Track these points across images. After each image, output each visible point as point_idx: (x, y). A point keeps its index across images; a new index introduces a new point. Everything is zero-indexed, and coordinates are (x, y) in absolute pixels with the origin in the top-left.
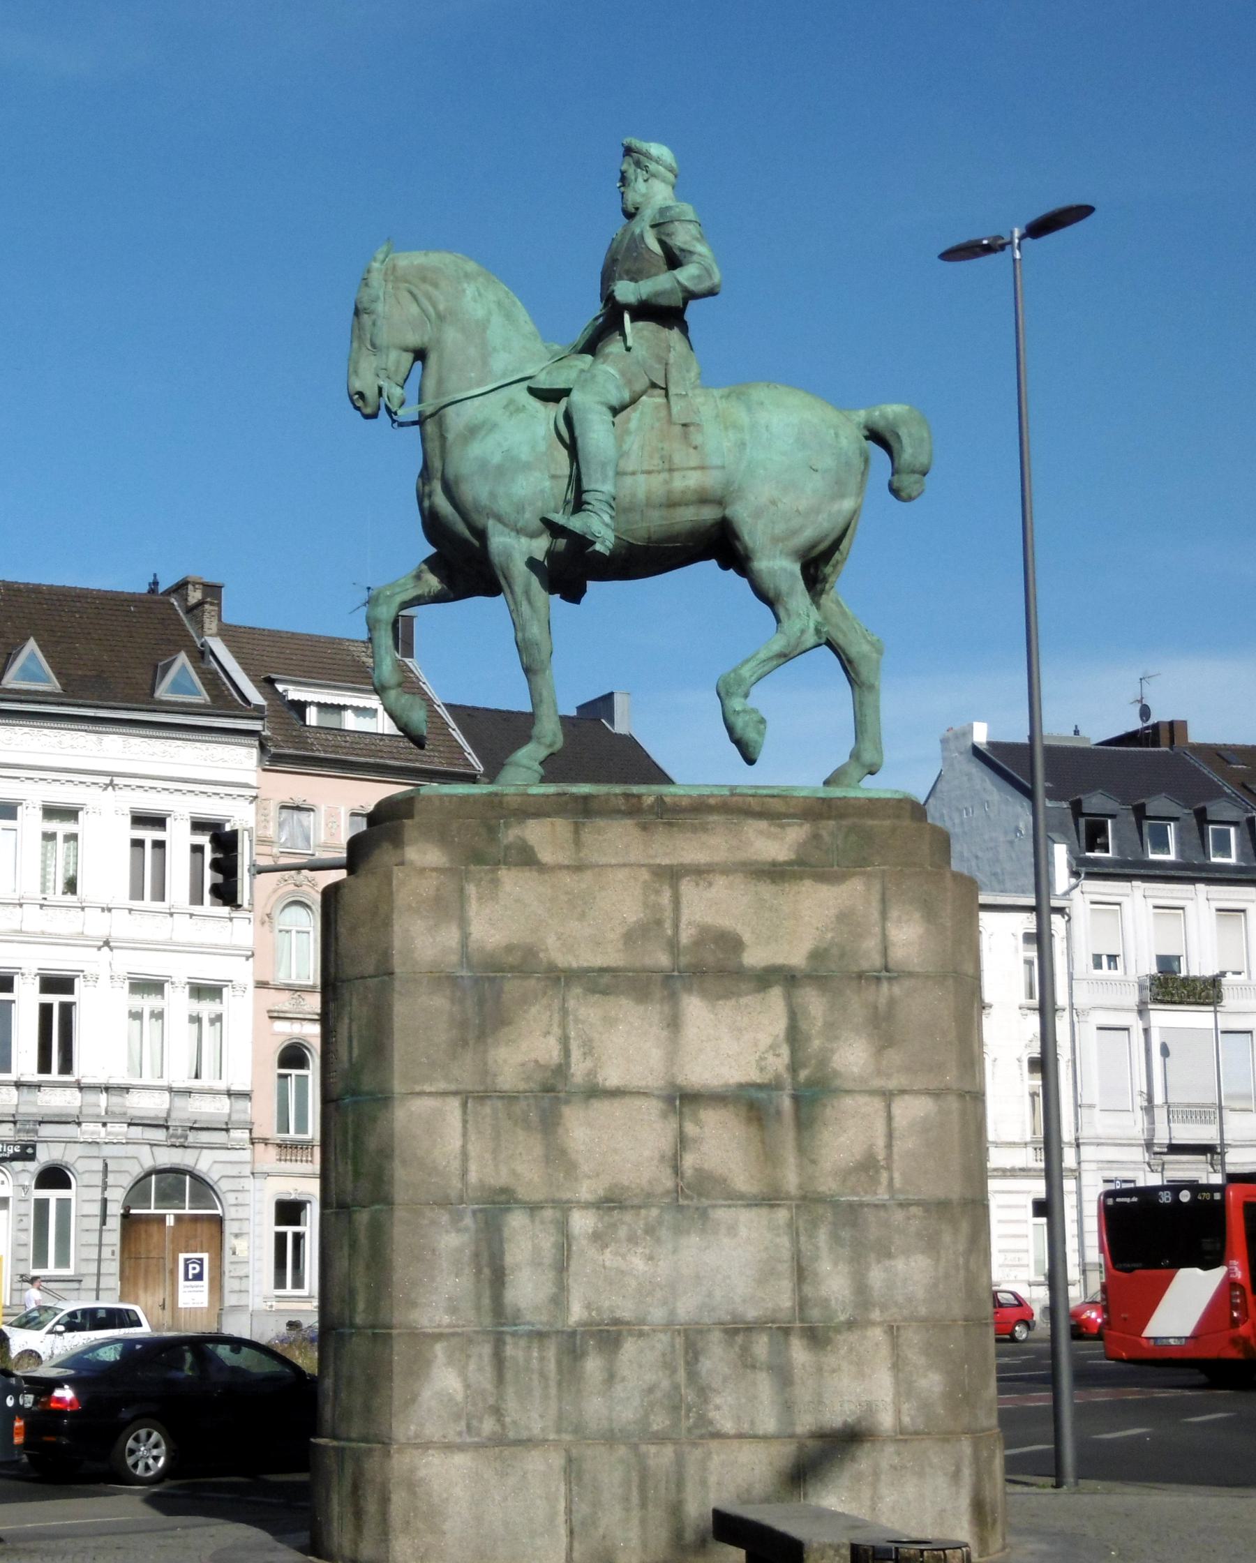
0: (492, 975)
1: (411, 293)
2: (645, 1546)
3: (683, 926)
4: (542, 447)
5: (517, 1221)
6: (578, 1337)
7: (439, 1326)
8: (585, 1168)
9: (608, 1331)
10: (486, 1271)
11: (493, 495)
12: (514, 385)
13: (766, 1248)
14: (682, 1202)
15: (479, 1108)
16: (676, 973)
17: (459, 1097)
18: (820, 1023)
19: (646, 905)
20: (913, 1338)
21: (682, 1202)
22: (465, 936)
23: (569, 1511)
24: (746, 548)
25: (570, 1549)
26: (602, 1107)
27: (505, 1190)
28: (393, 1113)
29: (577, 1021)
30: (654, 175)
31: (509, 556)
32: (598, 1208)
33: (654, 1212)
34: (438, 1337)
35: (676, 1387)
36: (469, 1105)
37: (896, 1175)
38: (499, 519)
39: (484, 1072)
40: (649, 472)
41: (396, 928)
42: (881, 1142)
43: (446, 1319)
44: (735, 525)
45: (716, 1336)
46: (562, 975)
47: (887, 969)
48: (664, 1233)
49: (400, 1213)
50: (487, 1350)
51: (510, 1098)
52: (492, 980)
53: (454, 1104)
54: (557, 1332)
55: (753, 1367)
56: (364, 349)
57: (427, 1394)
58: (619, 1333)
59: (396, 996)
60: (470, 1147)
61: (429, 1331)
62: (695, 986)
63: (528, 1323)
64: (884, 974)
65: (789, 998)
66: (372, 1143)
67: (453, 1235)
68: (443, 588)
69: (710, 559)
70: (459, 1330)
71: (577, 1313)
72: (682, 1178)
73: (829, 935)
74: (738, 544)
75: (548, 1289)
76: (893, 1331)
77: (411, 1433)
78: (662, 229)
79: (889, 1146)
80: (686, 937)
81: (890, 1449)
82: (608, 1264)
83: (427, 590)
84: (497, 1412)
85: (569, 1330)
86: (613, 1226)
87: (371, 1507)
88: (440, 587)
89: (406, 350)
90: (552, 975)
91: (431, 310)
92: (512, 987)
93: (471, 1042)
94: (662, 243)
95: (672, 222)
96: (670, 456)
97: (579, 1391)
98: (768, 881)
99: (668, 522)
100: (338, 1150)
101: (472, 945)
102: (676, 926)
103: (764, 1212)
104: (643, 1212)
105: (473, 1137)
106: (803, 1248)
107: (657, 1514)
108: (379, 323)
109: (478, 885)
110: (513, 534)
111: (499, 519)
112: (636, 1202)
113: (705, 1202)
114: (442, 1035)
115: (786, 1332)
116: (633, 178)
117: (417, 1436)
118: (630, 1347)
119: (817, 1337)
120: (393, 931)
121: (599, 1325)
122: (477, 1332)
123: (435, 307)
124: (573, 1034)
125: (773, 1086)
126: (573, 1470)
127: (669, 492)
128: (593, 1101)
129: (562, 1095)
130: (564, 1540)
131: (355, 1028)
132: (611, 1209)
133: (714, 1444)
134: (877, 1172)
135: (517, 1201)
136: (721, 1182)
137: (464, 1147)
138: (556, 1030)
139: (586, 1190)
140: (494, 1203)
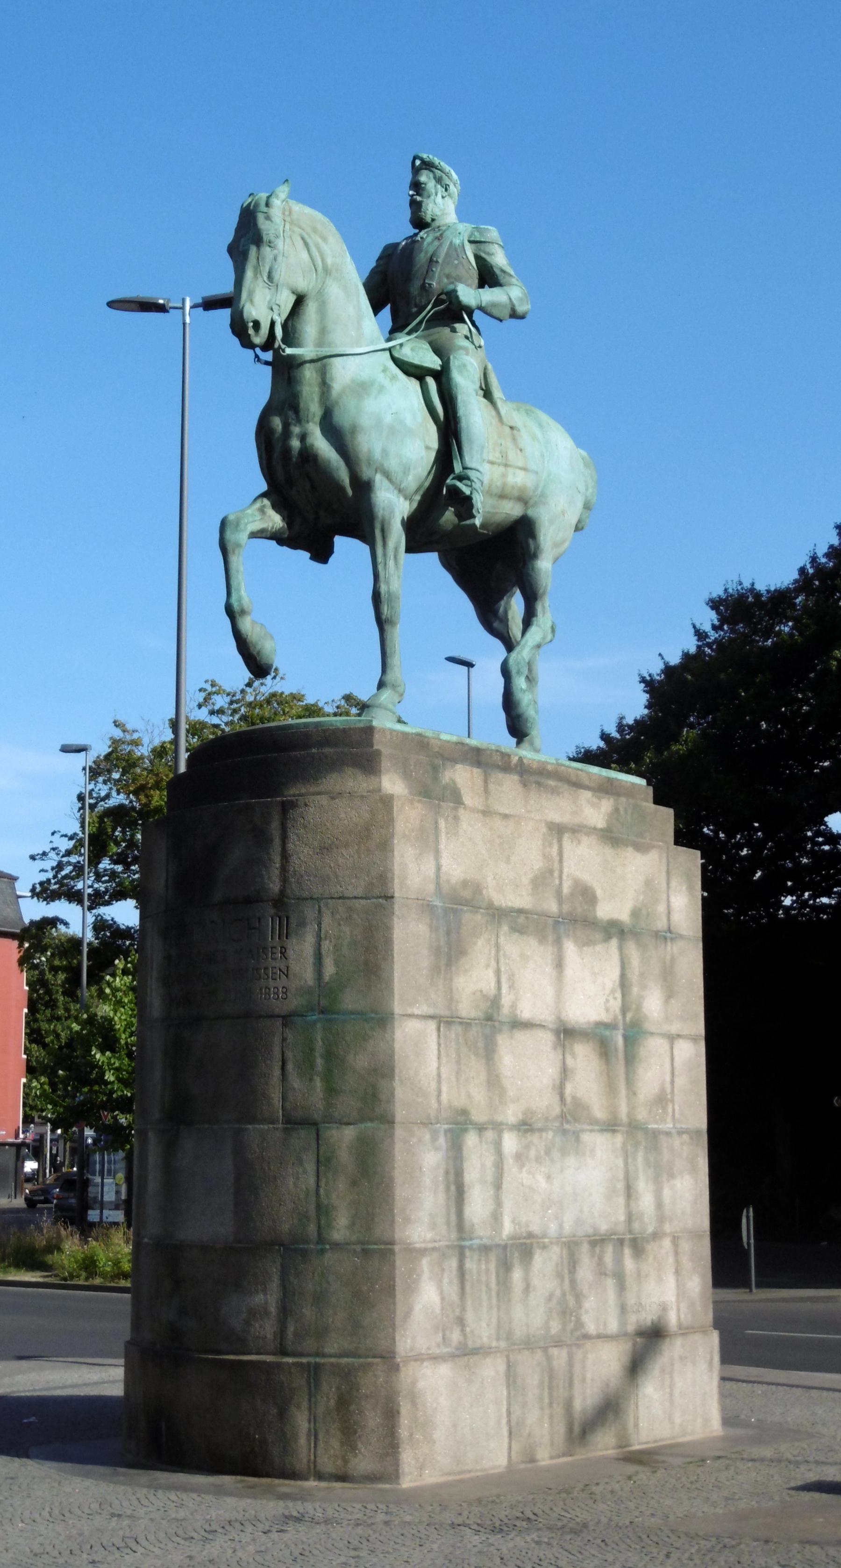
0: (455, 906)
1: (303, 239)
2: (552, 1443)
3: (564, 877)
4: (420, 420)
5: (471, 1140)
6: (508, 1250)
7: (424, 1241)
8: (511, 1093)
9: (525, 1244)
10: (453, 1188)
11: (385, 452)
12: (379, 353)
13: (611, 1169)
14: (566, 1126)
15: (448, 1033)
16: (560, 920)
17: (435, 1021)
18: (637, 973)
19: (544, 856)
20: (685, 1246)
21: (566, 1126)
22: (439, 868)
23: (509, 1413)
24: (537, 547)
25: (510, 1448)
26: (521, 1036)
27: (464, 1112)
28: (393, 1033)
29: (505, 955)
30: (449, 195)
31: (392, 512)
32: (519, 1130)
33: (550, 1134)
34: (423, 1252)
35: (564, 1294)
36: (442, 1029)
37: (677, 1108)
38: (387, 475)
39: (451, 999)
40: (492, 463)
41: (396, 853)
42: (668, 1078)
43: (429, 1235)
44: (537, 525)
45: (585, 1247)
46: (496, 912)
47: (669, 930)
48: (556, 1154)
49: (399, 1132)
50: (454, 1263)
51: (466, 1024)
52: (455, 911)
53: (432, 1025)
54: (497, 1246)
55: (605, 1274)
56: (260, 279)
57: (418, 1308)
58: (531, 1244)
59: (395, 919)
60: (443, 1070)
61: (418, 1246)
62: (571, 932)
63: (481, 1238)
64: (668, 935)
65: (621, 948)
66: (360, 1061)
67: (433, 1153)
68: (283, 527)
69: (333, 543)
70: (437, 1245)
71: (508, 1228)
72: (565, 1105)
73: (641, 897)
74: (531, 541)
75: (491, 1206)
76: (675, 1240)
77: (408, 1347)
78: (482, 246)
79: (672, 1082)
80: (566, 890)
81: (679, 1342)
82: (525, 1181)
83: (271, 525)
84: (461, 1322)
85: (503, 1243)
86: (527, 1147)
87: (372, 1419)
88: (281, 525)
89: (293, 293)
90: (490, 912)
91: (319, 263)
92: (471, 919)
93: (443, 968)
94: (478, 258)
95: (493, 243)
96: (507, 452)
97: (509, 1300)
98: (610, 845)
99: (494, 511)
100: (290, 1066)
101: (444, 878)
102: (561, 877)
103: (608, 1135)
104: (544, 1134)
105: (444, 1060)
106: (630, 1169)
107: (559, 1410)
108: (280, 259)
109: (446, 820)
110: (396, 492)
111: (387, 475)
112: (539, 1125)
113: (578, 1126)
114: (425, 960)
115: (621, 1242)
116: (433, 191)
117: (412, 1349)
118: (538, 1259)
119: (638, 1246)
120: (393, 856)
121: (519, 1239)
122: (448, 1247)
123: (323, 260)
124: (503, 969)
125: (609, 1026)
126: (511, 1376)
127: (504, 485)
128: (515, 1031)
129: (496, 1024)
130: (506, 1440)
131: (326, 946)
132: (526, 1131)
133: (588, 1344)
134: (666, 1104)
135: (471, 1123)
136: (586, 1108)
137: (439, 1068)
138: (493, 963)
139: (511, 1114)
140: (457, 1124)
